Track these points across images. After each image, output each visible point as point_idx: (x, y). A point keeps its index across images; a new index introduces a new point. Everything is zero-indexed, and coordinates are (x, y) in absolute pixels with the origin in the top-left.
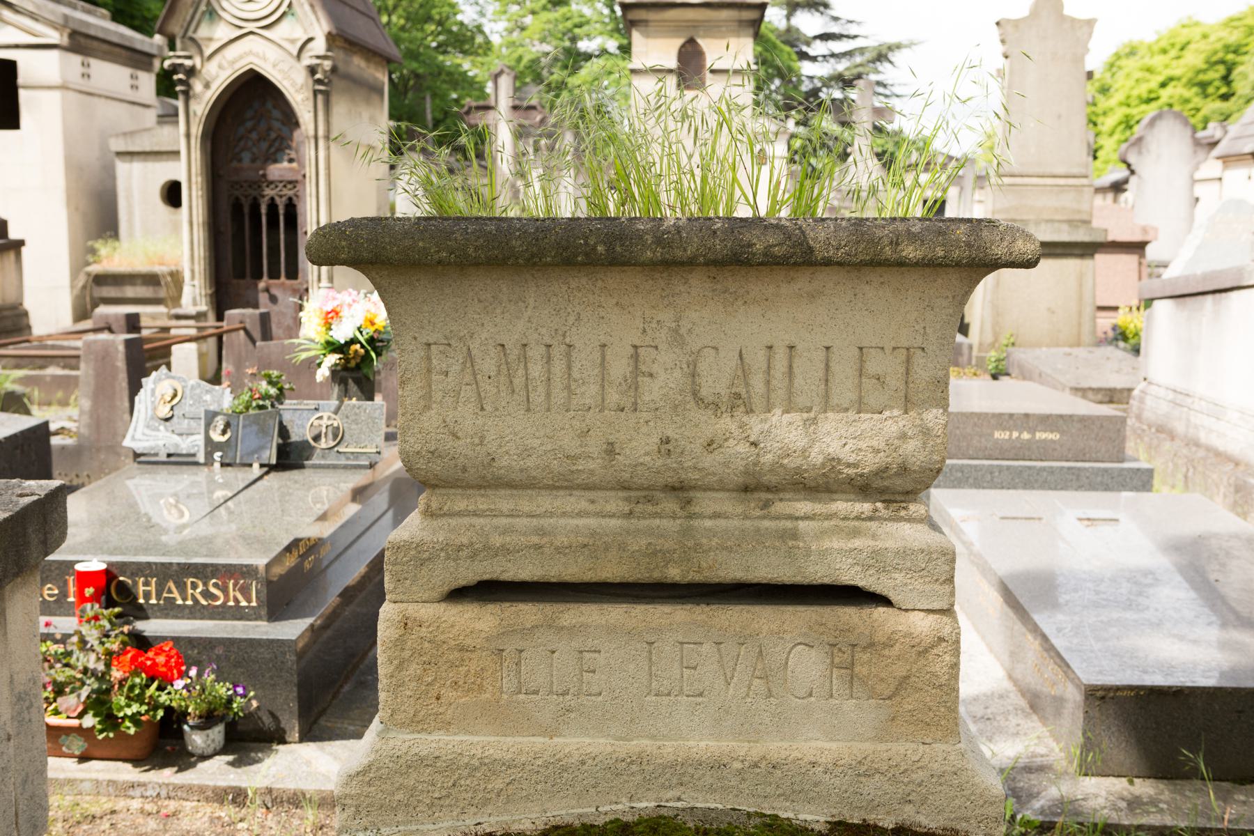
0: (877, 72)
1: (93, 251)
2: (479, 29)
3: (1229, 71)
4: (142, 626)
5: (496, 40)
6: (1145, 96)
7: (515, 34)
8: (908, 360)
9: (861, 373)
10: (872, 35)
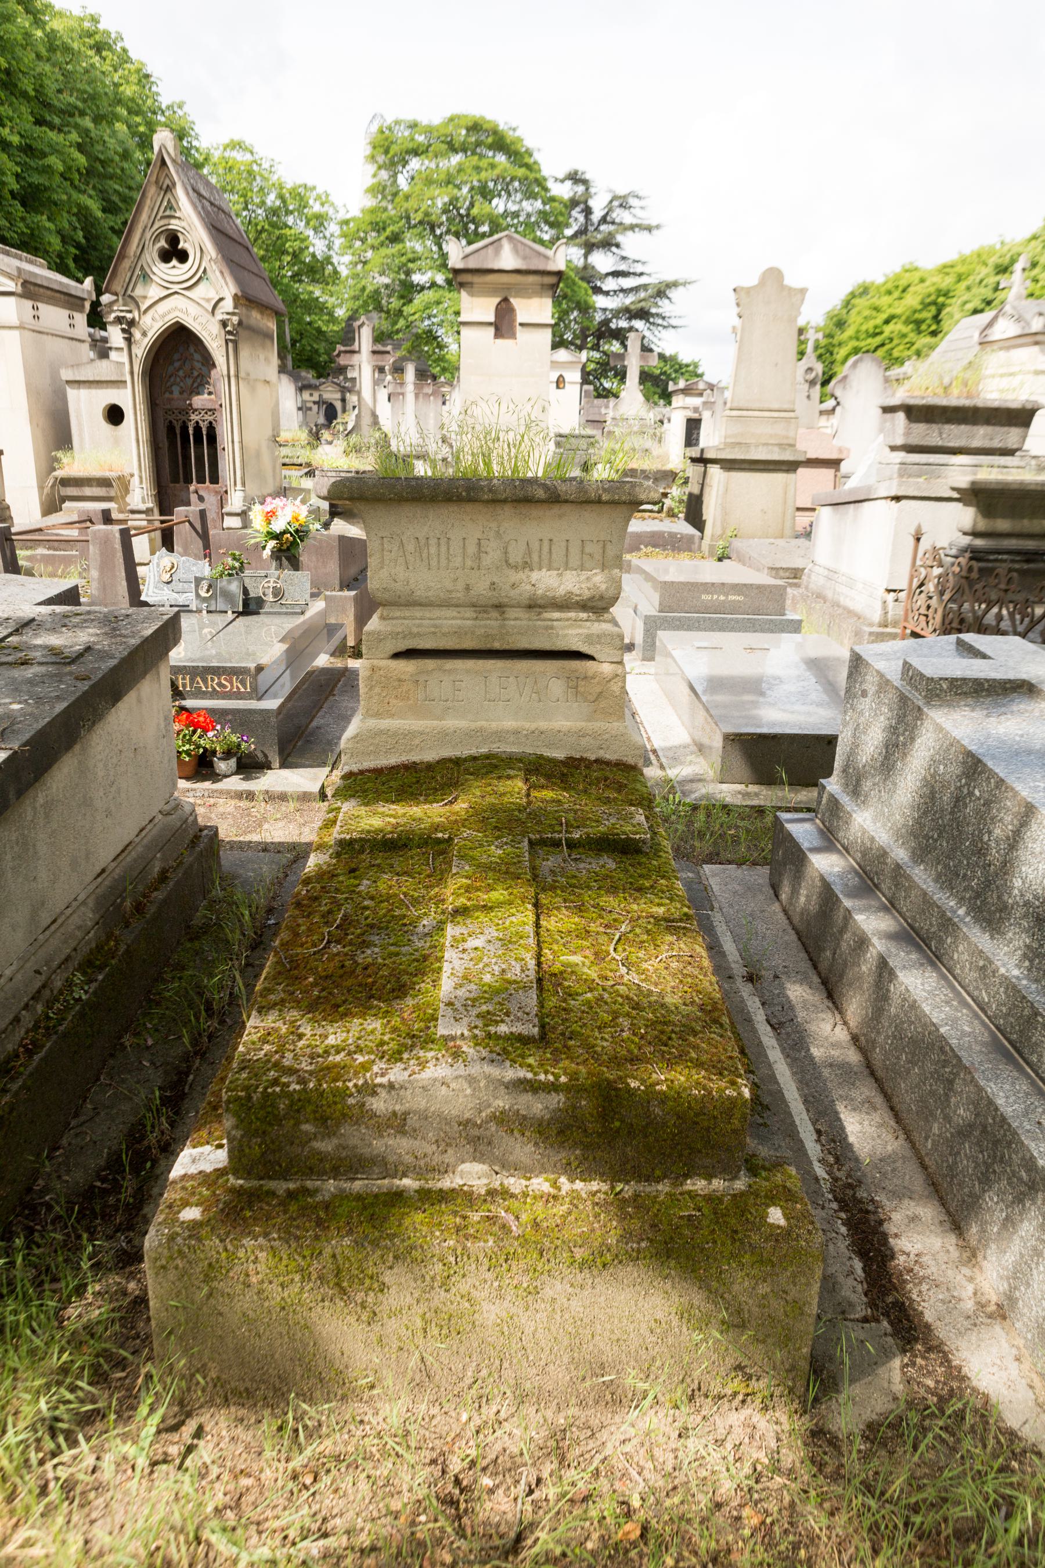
0: (656, 305)
1: (57, 460)
2: (328, 260)
3: (939, 312)
4: (184, 703)
5: (344, 271)
6: (871, 331)
7: (360, 266)
8: (604, 547)
9: (582, 552)
10: (657, 273)
